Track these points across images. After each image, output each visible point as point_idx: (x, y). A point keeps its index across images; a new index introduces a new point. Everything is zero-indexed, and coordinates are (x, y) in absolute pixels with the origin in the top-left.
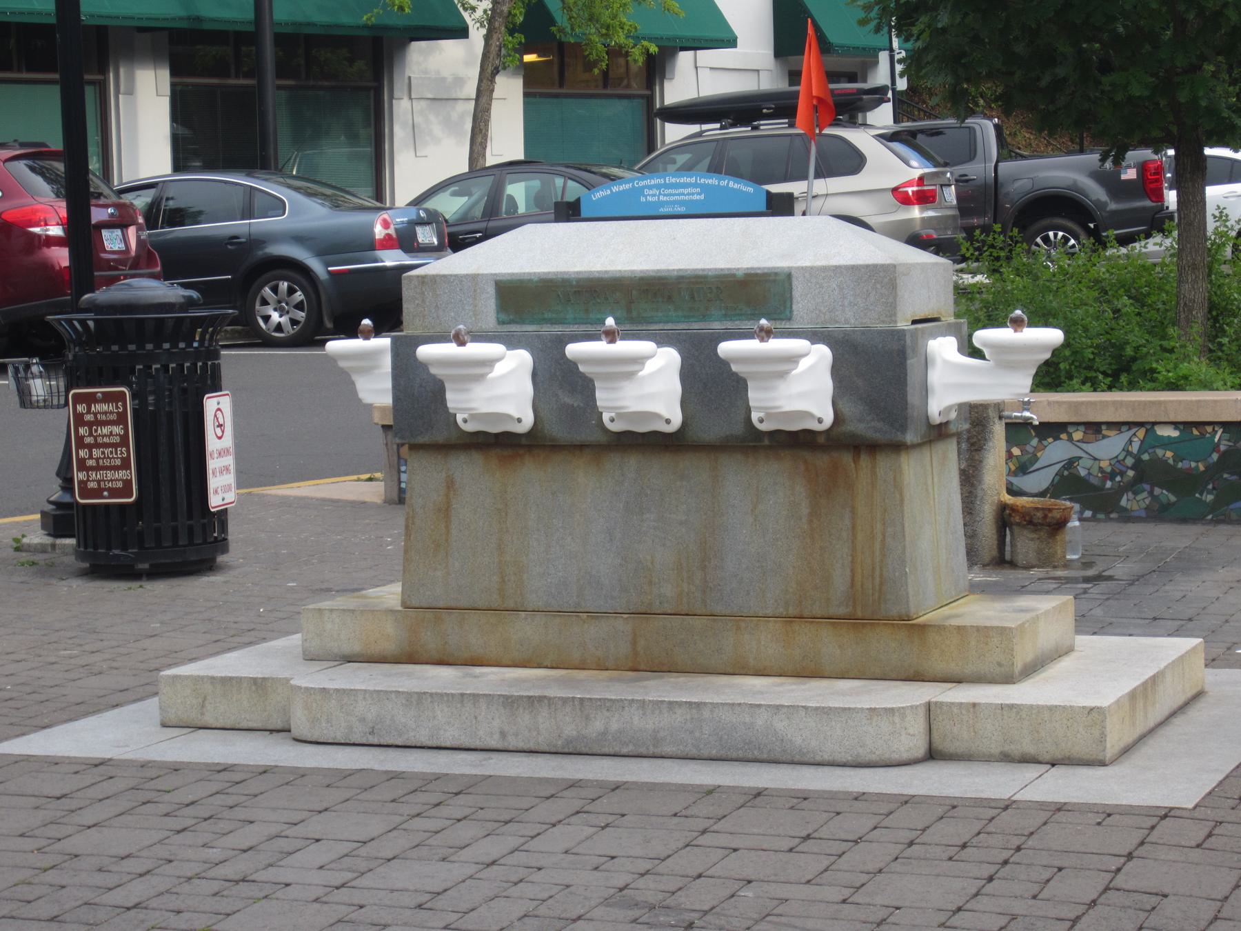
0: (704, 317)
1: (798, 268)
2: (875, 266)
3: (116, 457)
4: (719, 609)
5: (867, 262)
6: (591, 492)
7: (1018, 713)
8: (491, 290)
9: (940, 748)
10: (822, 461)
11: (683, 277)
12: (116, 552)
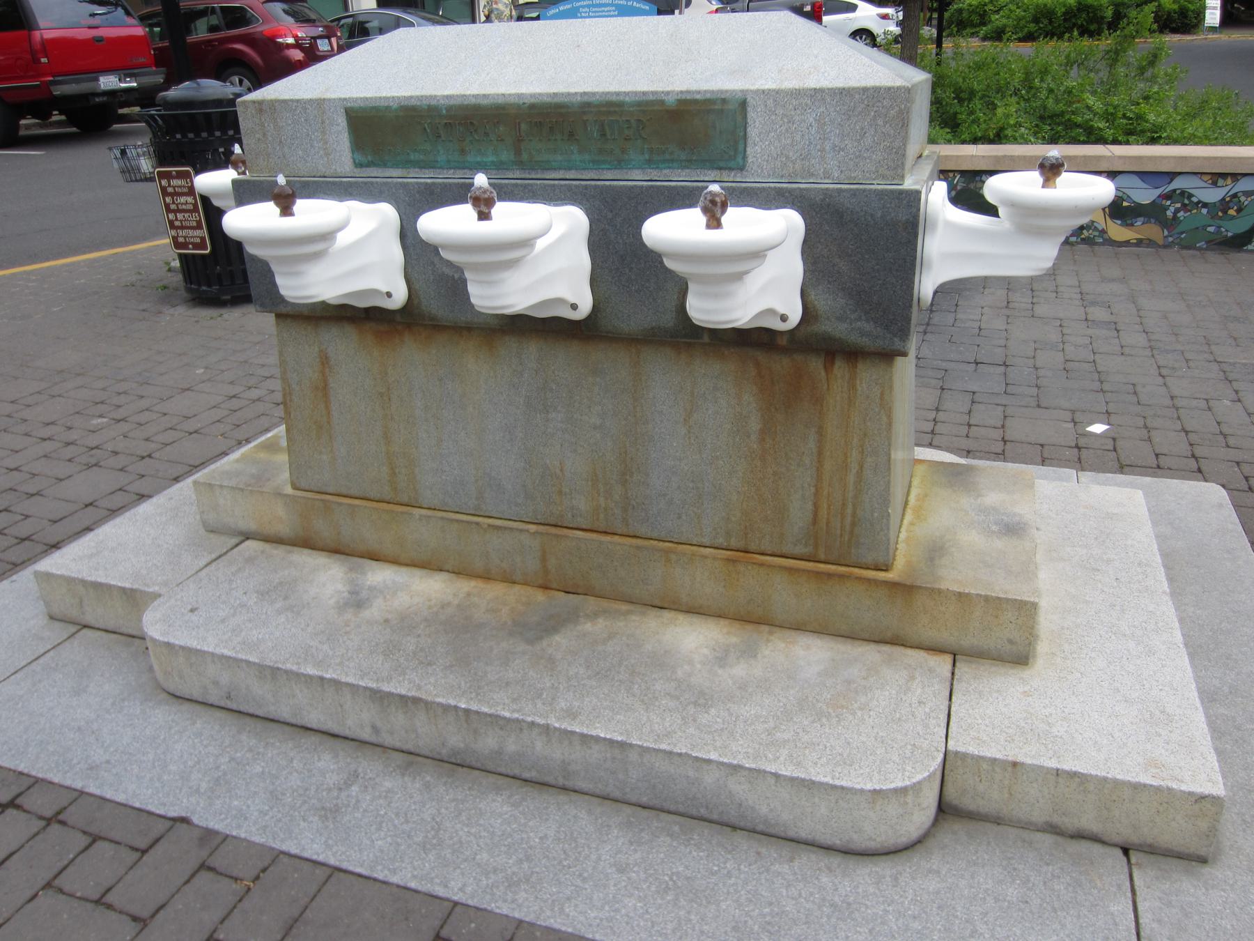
0: (620, 164)
1: (757, 92)
2: (877, 90)
3: (192, 219)
4: (643, 530)
5: (863, 84)
6: (485, 379)
7: (1082, 783)
8: (342, 122)
9: (955, 802)
10: (781, 365)
11: (588, 104)
12: (204, 288)
